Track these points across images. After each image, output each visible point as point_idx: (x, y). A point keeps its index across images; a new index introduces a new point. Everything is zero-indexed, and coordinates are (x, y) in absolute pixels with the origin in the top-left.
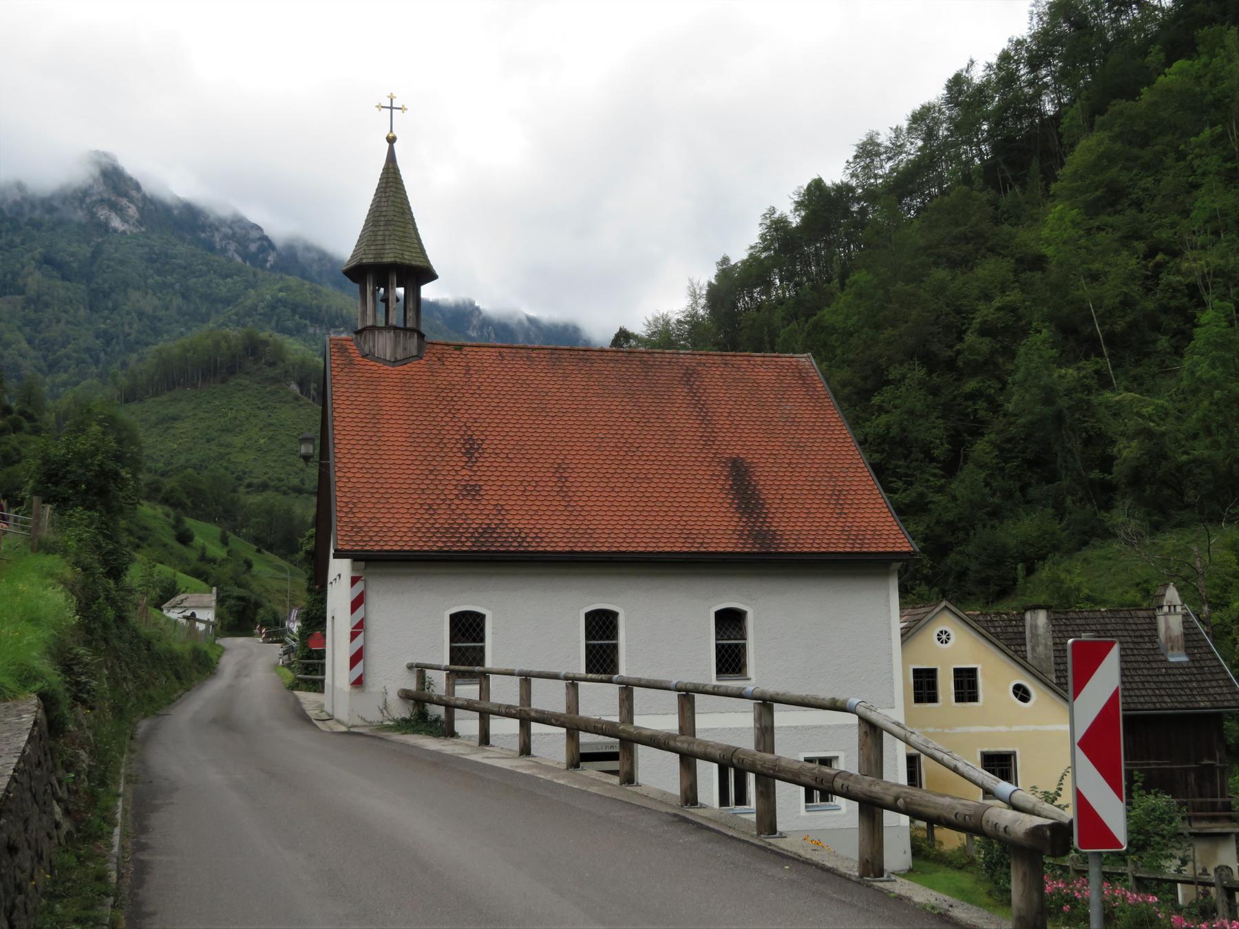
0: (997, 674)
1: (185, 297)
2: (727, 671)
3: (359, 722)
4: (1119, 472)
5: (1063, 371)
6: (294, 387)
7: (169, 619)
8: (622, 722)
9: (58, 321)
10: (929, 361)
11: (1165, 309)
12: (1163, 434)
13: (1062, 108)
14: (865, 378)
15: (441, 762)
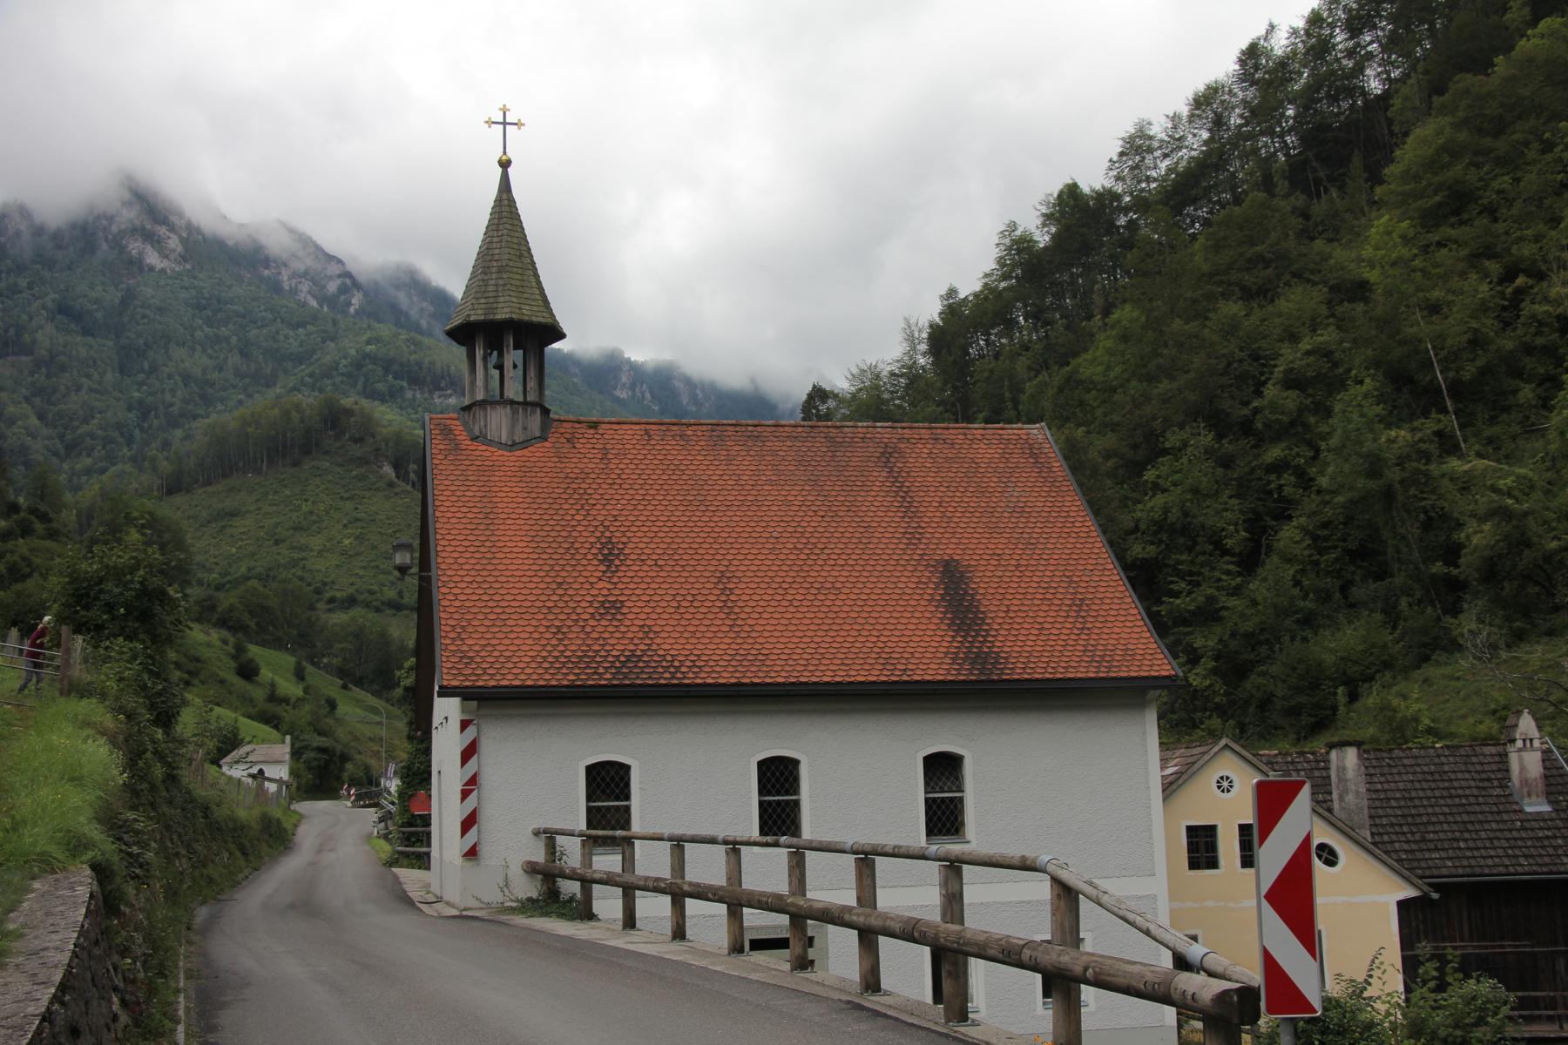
1: (243, 354)
2: (940, 833)
3: (472, 903)
4: (1468, 564)
5: (1393, 433)
6: (388, 470)
7: (230, 778)
8: (793, 894)
9: (79, 388)
10: (1219, 423)
11: (1529, 350)
12: (1526, 514)
13: (1392, 85)
14: (1135, 447)
15: (572, 948)
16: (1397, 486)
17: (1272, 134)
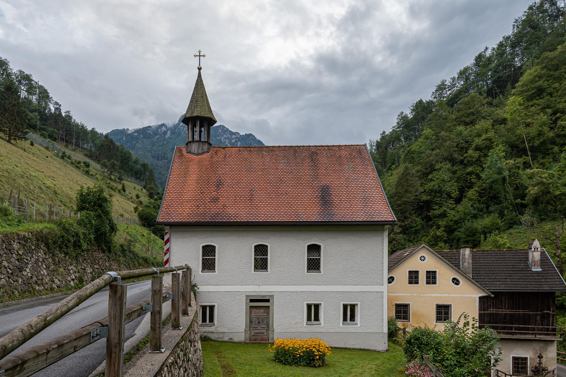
0: (445, 274)
10: (452, 161)
11: (558, 136)
12: (550, 184)
14: (426, 169)
16: (507, 177)
17: (483, 80)
